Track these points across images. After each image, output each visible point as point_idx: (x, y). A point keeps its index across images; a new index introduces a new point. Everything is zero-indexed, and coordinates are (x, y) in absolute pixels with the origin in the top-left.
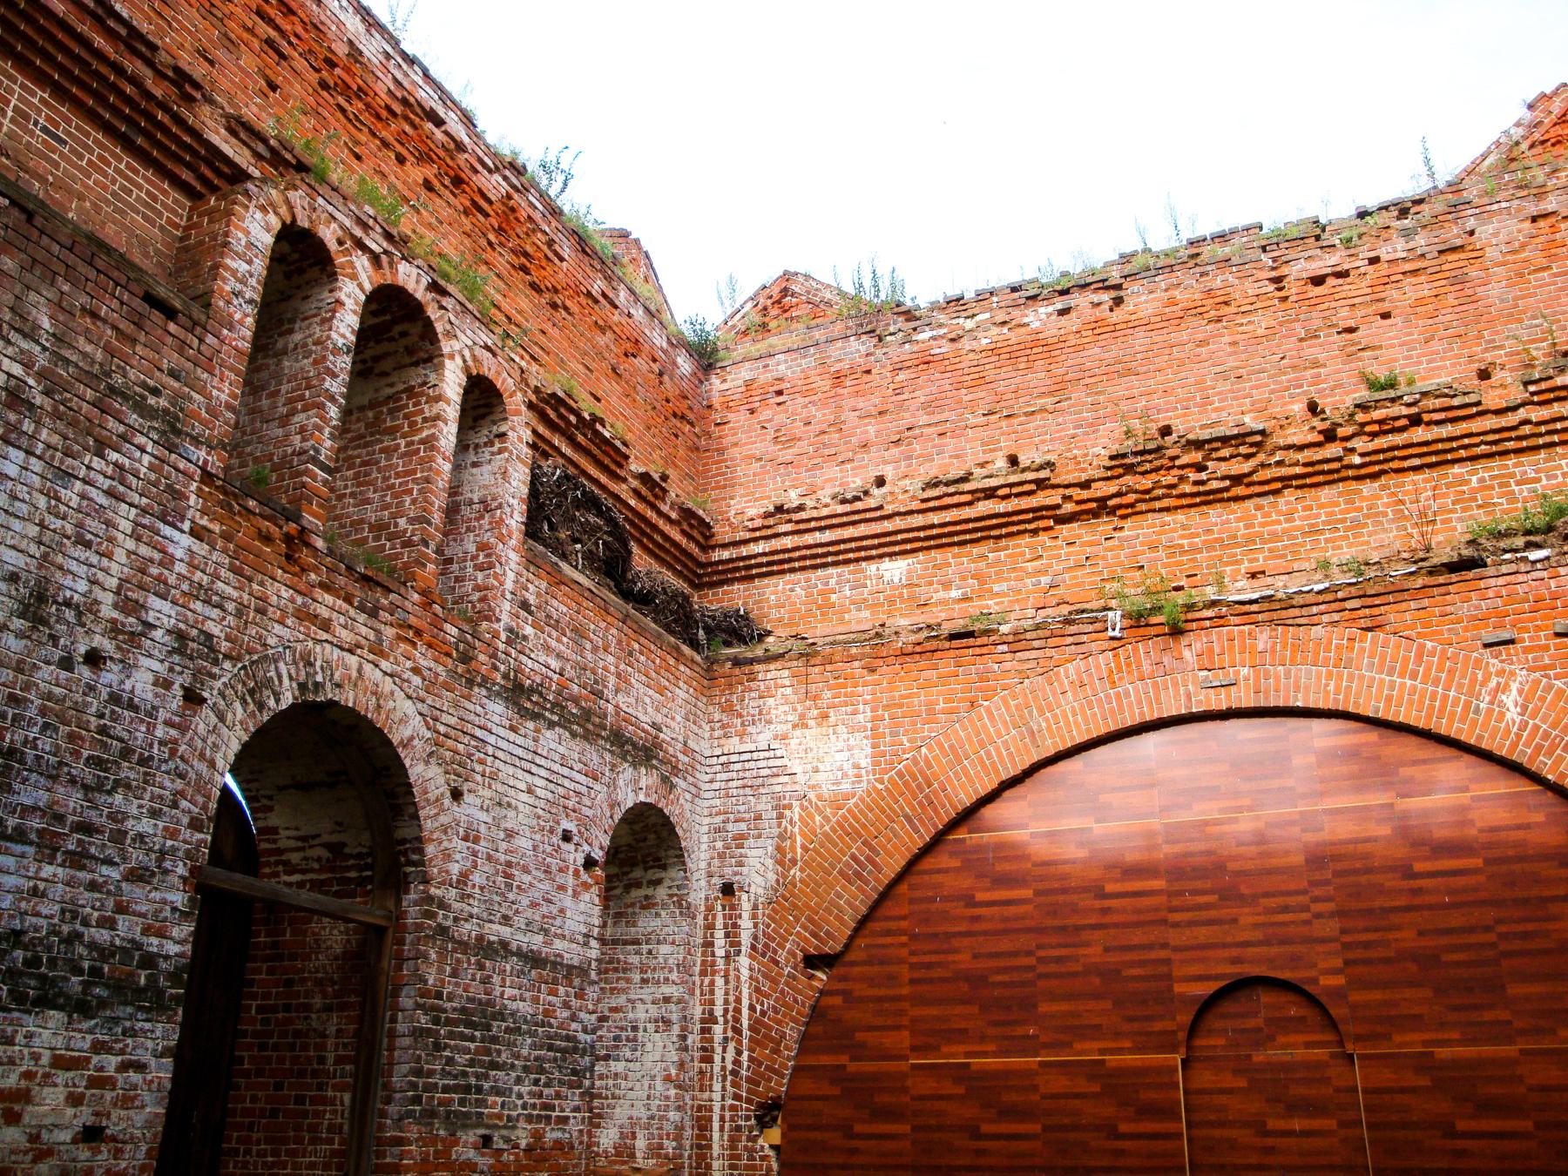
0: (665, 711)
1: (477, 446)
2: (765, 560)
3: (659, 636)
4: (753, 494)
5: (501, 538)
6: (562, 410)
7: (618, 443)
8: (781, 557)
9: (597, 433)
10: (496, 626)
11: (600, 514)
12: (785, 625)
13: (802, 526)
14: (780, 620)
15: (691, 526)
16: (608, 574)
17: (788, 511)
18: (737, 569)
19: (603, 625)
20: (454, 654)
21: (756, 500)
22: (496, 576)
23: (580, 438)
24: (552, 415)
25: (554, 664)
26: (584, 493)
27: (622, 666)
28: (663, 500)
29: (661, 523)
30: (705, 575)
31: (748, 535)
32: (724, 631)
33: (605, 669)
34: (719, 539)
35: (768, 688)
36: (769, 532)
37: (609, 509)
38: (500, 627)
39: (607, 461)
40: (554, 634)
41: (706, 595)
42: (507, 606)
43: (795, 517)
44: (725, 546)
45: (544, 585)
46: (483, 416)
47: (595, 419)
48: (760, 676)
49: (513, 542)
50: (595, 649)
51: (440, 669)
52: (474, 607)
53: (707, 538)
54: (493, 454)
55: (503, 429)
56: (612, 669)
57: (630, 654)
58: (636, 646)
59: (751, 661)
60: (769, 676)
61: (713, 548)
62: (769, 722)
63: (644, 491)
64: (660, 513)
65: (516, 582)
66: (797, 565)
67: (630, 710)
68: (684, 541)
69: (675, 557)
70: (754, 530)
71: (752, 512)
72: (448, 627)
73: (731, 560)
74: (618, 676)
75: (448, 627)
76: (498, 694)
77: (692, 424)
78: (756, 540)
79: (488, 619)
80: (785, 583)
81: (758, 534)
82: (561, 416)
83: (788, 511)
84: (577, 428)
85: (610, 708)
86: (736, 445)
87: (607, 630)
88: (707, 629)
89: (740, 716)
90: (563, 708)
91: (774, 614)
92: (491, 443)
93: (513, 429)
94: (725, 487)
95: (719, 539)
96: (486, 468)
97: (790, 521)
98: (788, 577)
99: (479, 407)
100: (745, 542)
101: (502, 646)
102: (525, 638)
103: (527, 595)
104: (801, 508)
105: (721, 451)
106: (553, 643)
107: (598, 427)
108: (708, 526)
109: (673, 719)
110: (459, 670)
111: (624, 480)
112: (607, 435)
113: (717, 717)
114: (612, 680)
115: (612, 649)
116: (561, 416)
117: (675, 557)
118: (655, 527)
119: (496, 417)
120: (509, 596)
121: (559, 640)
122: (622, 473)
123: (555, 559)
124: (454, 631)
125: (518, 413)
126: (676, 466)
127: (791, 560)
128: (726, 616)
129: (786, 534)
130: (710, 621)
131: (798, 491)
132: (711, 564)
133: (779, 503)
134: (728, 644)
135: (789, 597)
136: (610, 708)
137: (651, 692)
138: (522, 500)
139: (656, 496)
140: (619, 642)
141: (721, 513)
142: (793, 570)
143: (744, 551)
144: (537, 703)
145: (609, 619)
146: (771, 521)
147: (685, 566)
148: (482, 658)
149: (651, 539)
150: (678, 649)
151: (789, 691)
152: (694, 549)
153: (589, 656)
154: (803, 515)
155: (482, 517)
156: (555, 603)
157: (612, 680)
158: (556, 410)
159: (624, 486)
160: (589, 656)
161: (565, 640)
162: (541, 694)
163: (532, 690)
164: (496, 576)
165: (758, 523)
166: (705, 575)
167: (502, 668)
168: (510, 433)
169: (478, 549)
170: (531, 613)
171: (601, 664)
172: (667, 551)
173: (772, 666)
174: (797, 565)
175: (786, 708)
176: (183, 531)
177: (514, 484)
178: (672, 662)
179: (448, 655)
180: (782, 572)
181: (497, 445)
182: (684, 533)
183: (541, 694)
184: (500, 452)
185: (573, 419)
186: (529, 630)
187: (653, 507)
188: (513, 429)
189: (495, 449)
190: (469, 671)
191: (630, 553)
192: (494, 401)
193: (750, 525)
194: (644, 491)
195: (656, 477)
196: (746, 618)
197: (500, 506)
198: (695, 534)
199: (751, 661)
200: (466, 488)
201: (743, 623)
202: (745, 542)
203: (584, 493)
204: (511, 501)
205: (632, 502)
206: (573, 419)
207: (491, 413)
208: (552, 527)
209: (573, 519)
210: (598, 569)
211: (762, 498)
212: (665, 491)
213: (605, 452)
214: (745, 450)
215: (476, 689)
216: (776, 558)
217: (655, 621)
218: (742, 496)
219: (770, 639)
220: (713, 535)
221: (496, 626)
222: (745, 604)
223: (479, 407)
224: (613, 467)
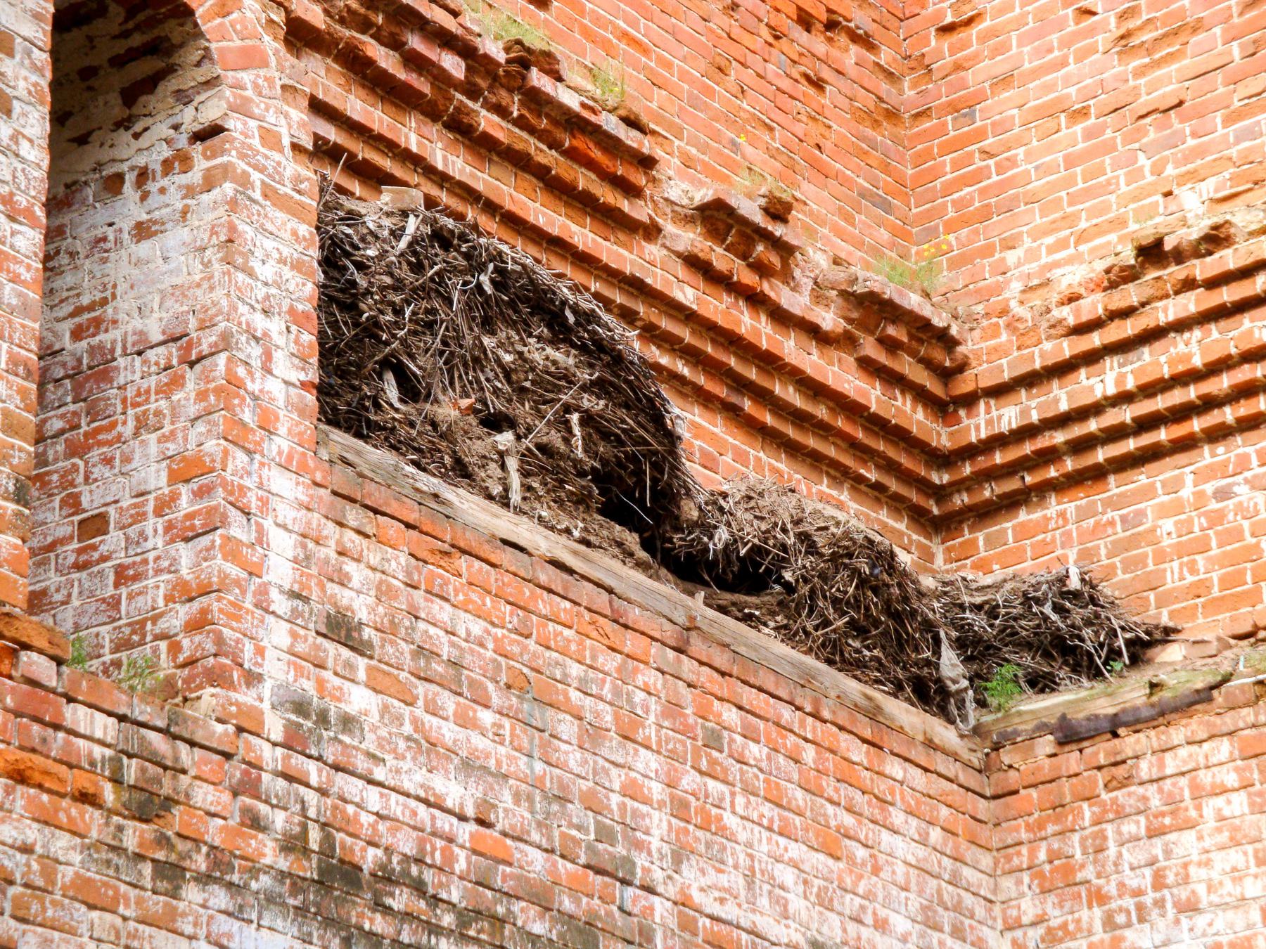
0: (851, 903)
1: (143, 175)
2: (1126, 414)
3: (807, 681)
4: (1070, 220)
5: (237, 437)
6: (415, 42)
7: (611, 123)
8: (1177, 397)
9: (535, 99)
10: (246, 697)
11: (560, 333)
12: (1216, 605)
13: (1227, 295)
14: (1199, 589)
15: (891, 346)
16: (615, 512)
17: (1179, 256)
18: (1049, 456)
19: (611, 662)
20: (109, 794)
21: (1081, 238)
22: (232, 551)
23: (487, 121)
24: (385, 59)
25: (454, 791)
26: (502, 279)
27: (690, 780)
28: (786, 276)
29: (791, 348)
30: (960, 485)
31: (1068, 348)
32: (1028, 646)
33: (632, 791)
34: (982, 374)
35: (1173, 802)
36: (1129, 328)
37: (587, 318)
38: (260, 699)
39: (584, 180)
40: (449, 702)
41: (967, 551)
42: (278, 635)
43: (1201, 268)
44: (1000, 391)
45: (399, 562)
46: (150, 84)
47: (524, 58)
48: (1145, 768)
49: (281, 444)
50: (591, 736)
51: (61, 844)
52: (175, 648)
53: (947, 375)
54: (190, 191)
55: (211, 110)
56: (657, 790)
57: (713, 743)
58: (731, 716)
59: (1113, 727)
60: (1171, 764)
61: (970, 401)
62: (1190, 907)
63: (721, 258)
64: (781, 317)
65: (303, 561)
66: (1228, 415)
67: (729, 911)
68: (872, 395)
69: (854, 446)
70: (1082, 329)
71: (1072, 277)
72: (77, 716)
73: (1027, 432)
74: (680, 809)
75: (77, 716)
76: (271, 899)
77: (864, 40)
78: (1091, 358)
79: (218, 678)
80: (1202, 476)
81: (1096, 340)
82: (414, 61)
83: (1179, 256)
84: (474, 93)
85: (661, 909)
86: (1004, 81)
87: (624, 677)
88: (972, 648)
89: (1099, 897)
90: (499, 922)
91: (1174, 575)
92: (179, 161)
93: (242, 109)
94: (985, 214)
95: (982, 374)
96: (176, 237)
97: (1188, 284)
98: (1208, 455)
99: (134, 55)
100: (1063, 369)
101: (271, 756)
102: (348, 722)
103: (345, 597)
104: (1216, 239)
105: (962, 108)
106: (449, 732)
107: (537, 78)
108: (946, 340)
109: (881, 925)
110: (130, 841)
111: (651, 232)
112: (571, 100)
113: (1029, 908)
114: (658, 825)
115: (649, 731)
116: (414, 61)
117: (854, 446)
118: (770, 362)
119: (188, 78)
120: (281, 604)
121: (465, 722)
122: (639, 211)
123: (428, 482)
124: (103, 726)
125: (252, 59)
126: (824, 173)
127: (1209, 403)
128: (1027, 600)
129: (1181, 326)
130: (979, 621)
131: (1209, 187)
132: (970, 451)
133: (1147, 238)
134: (1041, 683)
135: (1216, 518)
136: (661, 909)
137: (795, 850)
138: (295, 317)
139: (762, 269)
140: (673, 707)
141: (984, 295)
142: (1218, 434)
143: (1061, 397)
144: (407, 916)
145: (631, 642)
146: (1131, 294)
147: (890, 467)
148: (205, 795)
149: (763, 396)
150: (874, 714)
151: (1238, 804)
152: (914, 417)
153: (574, 758)
154: (1228, 259)
155: (177, 382)
156: (444, 612)
157: (658, 825)
158: (395, 44)
159: (653, 250)
160: (574, 758)
161: (486, 717)
162: (419, 887)
163: (386, 877)
164: (232, 551)
165: (1094, 305)
166: (960, 485)
167: (279, 820)
168: (234, 123)
169: (176, 477)
170: (360, 648)
171: (617, 778)
172: (823, 429)
173: (1177, 734)
174: (1228, 415)
175: (1235, 857)
176: (446, 719)
177: (266, 272)
178: (859, 752)
179: (87, 798)
180: (1186, 444)
181: (201, 164)
182: (868, 366)
183: (419, 887)
184: (209, 183)
185: (453, 65)
186: (360, 700)
187: (755, 300)
188: (242, 109)
189: (195, 176)
190: (163, 841)
191: (672, 439)
192: (172, 30)
193: (1069, 315)
194: (721, 258)
195: (751, 210)
196: (1088, 596)
197: (226, 342)
198: (907, 366)
199: (1113, 727)
200: (123, 306)
201: (1079, 614)
202: (1063, 369)
203: (502, 279)
204: (260, 322)
205: (688, 294)
206: (453, 65)
207: (170, 70)
208: (411, 390)
209: (478, 360)
210: (581, 500)
211: (1098, 230)
212: (785, 249)
213: (572, 155)
214: (1035, 95)
215: (192, 893)
216: (1161, 403)
217: (787, 634)
218: (1037, 234)
219: (1173, 653)
220: (962, 367)
221: (246, 697)
222: (1086, 555)
223: (134, 55)
224: (607, 195)
